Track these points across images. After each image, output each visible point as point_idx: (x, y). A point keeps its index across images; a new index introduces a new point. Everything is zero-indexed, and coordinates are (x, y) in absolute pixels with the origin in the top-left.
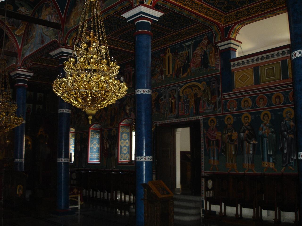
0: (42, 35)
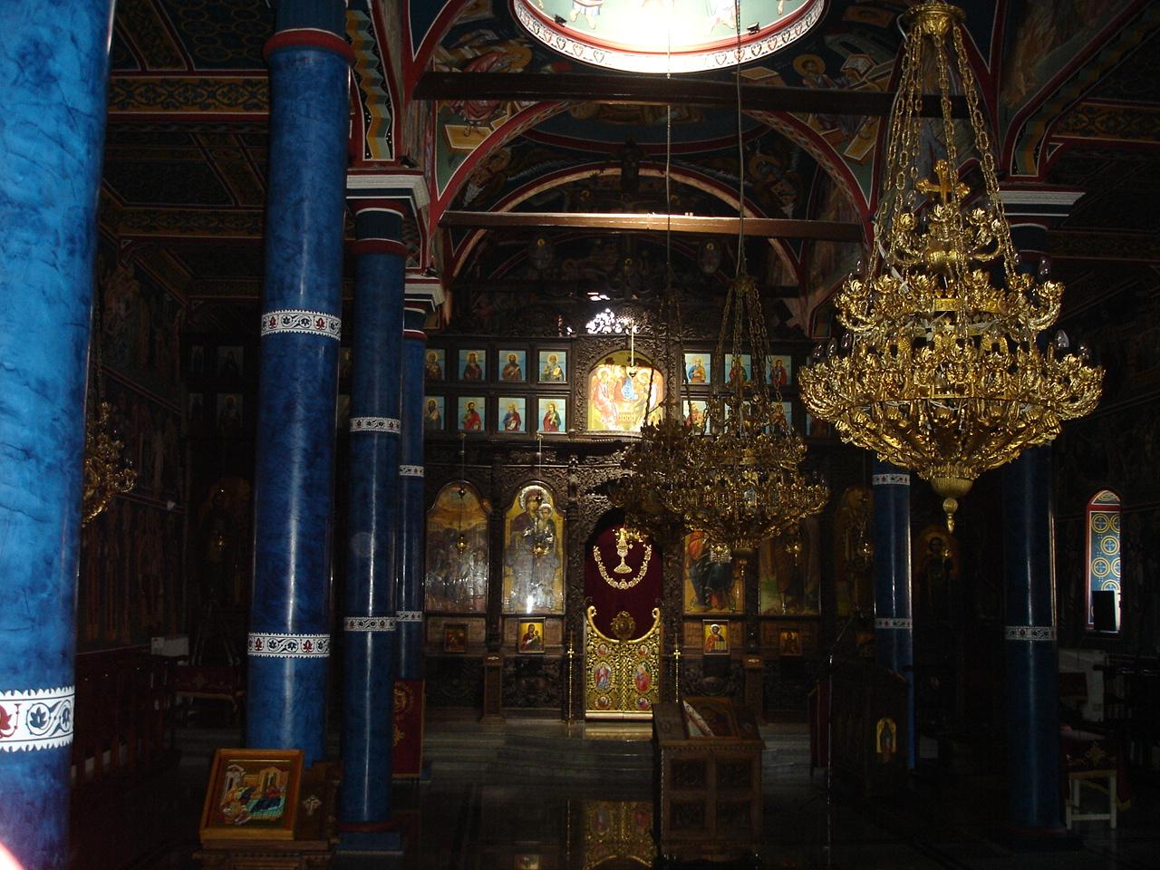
0: (931, 148)
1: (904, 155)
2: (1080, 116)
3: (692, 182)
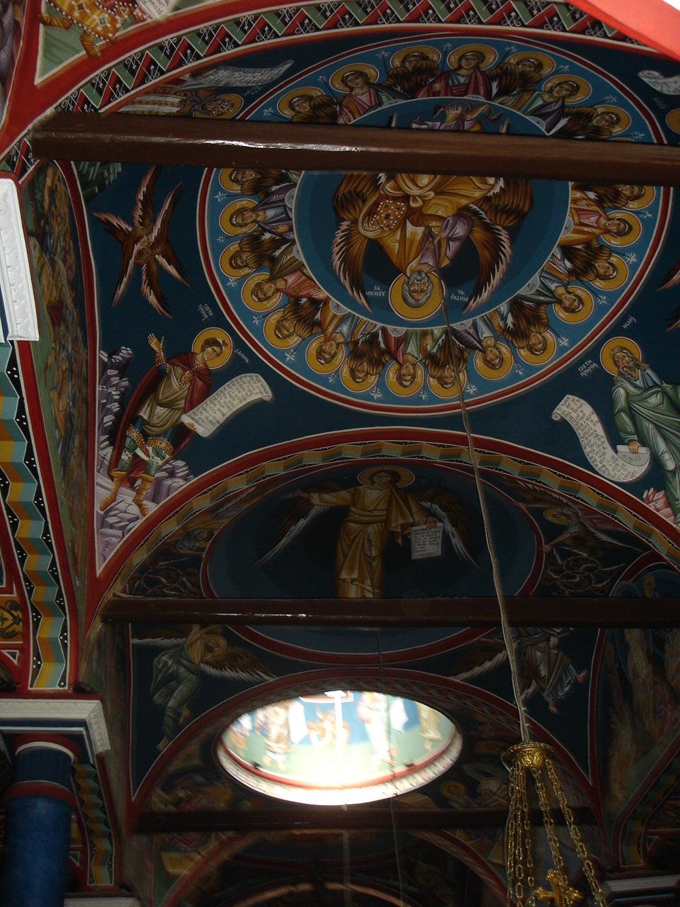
1: (519, 868)
2: (669, 812)
3: (372, 892)
